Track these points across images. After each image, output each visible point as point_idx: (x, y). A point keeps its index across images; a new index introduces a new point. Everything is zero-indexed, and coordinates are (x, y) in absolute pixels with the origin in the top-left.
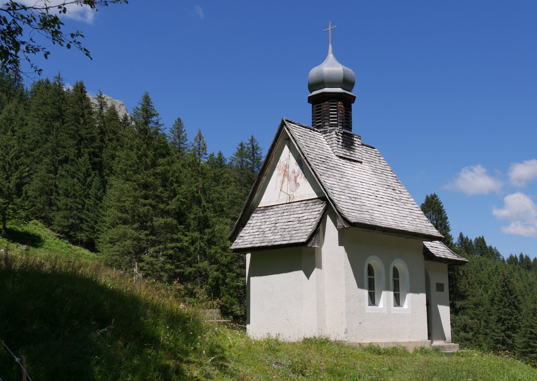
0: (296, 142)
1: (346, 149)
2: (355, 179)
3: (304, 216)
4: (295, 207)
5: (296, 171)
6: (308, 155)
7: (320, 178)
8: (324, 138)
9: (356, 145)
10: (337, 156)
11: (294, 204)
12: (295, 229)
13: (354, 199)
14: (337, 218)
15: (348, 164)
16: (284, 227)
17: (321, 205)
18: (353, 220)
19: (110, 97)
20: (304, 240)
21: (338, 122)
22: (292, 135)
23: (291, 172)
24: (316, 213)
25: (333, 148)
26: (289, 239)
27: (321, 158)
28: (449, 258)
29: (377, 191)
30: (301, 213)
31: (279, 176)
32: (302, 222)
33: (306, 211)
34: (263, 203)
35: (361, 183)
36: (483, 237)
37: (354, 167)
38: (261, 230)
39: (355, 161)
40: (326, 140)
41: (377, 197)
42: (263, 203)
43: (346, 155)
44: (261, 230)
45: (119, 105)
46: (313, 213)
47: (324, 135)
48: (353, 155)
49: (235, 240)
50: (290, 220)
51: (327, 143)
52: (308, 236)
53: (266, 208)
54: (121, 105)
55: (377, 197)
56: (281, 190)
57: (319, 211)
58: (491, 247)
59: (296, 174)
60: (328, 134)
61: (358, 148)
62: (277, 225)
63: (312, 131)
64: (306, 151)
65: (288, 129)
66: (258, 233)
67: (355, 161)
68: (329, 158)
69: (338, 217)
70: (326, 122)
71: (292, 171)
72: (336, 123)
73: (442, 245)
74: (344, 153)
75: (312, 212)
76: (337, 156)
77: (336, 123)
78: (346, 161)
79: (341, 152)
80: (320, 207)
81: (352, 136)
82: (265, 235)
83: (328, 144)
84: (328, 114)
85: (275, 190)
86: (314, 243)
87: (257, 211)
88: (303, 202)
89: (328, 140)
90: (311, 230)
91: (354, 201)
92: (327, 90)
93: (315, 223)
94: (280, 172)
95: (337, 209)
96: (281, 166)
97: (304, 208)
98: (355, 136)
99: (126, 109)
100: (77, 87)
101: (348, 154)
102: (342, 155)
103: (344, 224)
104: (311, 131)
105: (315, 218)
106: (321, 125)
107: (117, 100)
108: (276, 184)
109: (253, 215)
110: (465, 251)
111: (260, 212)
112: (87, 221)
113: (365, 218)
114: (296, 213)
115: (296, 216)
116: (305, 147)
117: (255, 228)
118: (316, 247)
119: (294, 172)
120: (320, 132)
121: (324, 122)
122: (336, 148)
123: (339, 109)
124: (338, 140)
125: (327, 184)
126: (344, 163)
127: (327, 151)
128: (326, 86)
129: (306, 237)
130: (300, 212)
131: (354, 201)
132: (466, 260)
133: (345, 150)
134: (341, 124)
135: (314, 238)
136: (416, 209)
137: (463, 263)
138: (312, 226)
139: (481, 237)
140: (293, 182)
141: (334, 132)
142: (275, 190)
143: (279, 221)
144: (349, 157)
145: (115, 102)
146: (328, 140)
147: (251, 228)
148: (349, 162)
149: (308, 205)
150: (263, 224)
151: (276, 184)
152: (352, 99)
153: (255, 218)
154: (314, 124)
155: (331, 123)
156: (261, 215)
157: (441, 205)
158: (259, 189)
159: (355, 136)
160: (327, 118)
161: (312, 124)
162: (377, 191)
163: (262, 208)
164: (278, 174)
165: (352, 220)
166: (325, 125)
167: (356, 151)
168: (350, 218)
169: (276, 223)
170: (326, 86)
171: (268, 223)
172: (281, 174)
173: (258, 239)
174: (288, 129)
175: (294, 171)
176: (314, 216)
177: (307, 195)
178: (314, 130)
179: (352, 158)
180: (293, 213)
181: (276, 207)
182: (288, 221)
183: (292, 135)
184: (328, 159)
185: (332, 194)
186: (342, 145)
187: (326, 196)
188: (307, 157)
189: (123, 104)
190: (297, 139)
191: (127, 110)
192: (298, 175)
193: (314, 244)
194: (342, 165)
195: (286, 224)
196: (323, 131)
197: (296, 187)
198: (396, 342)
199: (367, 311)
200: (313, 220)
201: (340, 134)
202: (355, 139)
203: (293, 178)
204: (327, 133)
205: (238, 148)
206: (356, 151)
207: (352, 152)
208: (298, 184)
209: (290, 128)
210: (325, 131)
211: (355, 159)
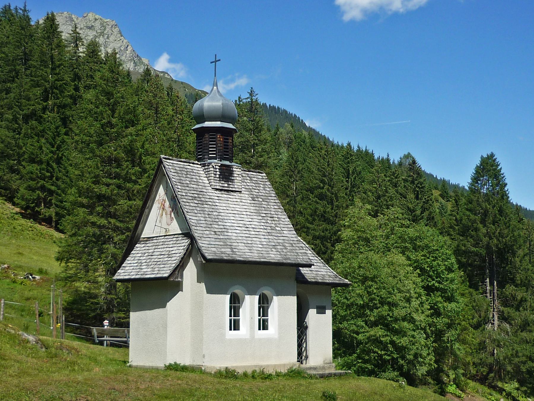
0: (169, 180)
2: (227, 211)
9: (235, 175)
10: (212, 188)
13: (219, 233)
15: (225, 196)
17: (187, 240)
18: (209, 257)
19: (99, 15)
20: (166, 275)
33: (175, 245)
39: (232, 191)
42: (145, 234)
43: (223, 187)
45: (110, 26)
47: (203, 168)
49: (119, 270)
51: (205, 176)
53: (149, 238)
54: (114, 26)
60: (206, 167)
61: (238, 178)
63: (191, 165)
65: (164, 167)
67: (232, 191)
72: (215, 156)
74: (221, 185)
76: (212, 188)
77: (215, 156)
78: (223, 192)
79: (218, 184)
80: (186, 242)
84: (207, 148)
86: (178, 277)
87: (141, 241)
89: (206, 173)
90: (174, 265)
91: (219, 235)
92: (207, 124)
95: (197, 246)
98: (235, 167)
99: (120, 31)
100: (48, 18)
101: (226, 185)
102: (218, 187)
103: (202, 260)
107: (108, 20)
109: (137, 245)
110: (393, 261)
111: (143, 243)
112: (57, 194)
113: (226, 253)
120: (200, 165)
121: (204, 155)
123: (219, 142)
124: (215, 173)
125: (192, 221)
128: (206, 120)
129: (169, 272)
131: (219, 235)
132: (349, 282)
133: (223, 182)
135: (177, 272)
136: (293, 236)
138: (175, 262)
143: (154, 254)
144: (226, 188)
145: (106, 22)
146: (206, 173)
148: (227, 193)
153: (138, 249)
155: (210, 156)
156: (143, 245)
158: (143, 221)
159: (235, 167)
163: (145, 239)
166: (204, 158)
167: (236, 181)
170: (206, 120)
171: (146, 254)
174: (164, 167)
179: (230, 189)
181: (155, 238)
186: (219, 178)
189: (116, 25)
191: (120, 33)
193: (177, 278)
196: (203, 164)
198: (258, 365)
199: (227, 337)
200: (178, 255)
201: (217, 167)
202: (234, 169)
204: (206, 166)
206: (236, 181)
207: (230, 183)
210: (204, 164)
211: (234, 189)
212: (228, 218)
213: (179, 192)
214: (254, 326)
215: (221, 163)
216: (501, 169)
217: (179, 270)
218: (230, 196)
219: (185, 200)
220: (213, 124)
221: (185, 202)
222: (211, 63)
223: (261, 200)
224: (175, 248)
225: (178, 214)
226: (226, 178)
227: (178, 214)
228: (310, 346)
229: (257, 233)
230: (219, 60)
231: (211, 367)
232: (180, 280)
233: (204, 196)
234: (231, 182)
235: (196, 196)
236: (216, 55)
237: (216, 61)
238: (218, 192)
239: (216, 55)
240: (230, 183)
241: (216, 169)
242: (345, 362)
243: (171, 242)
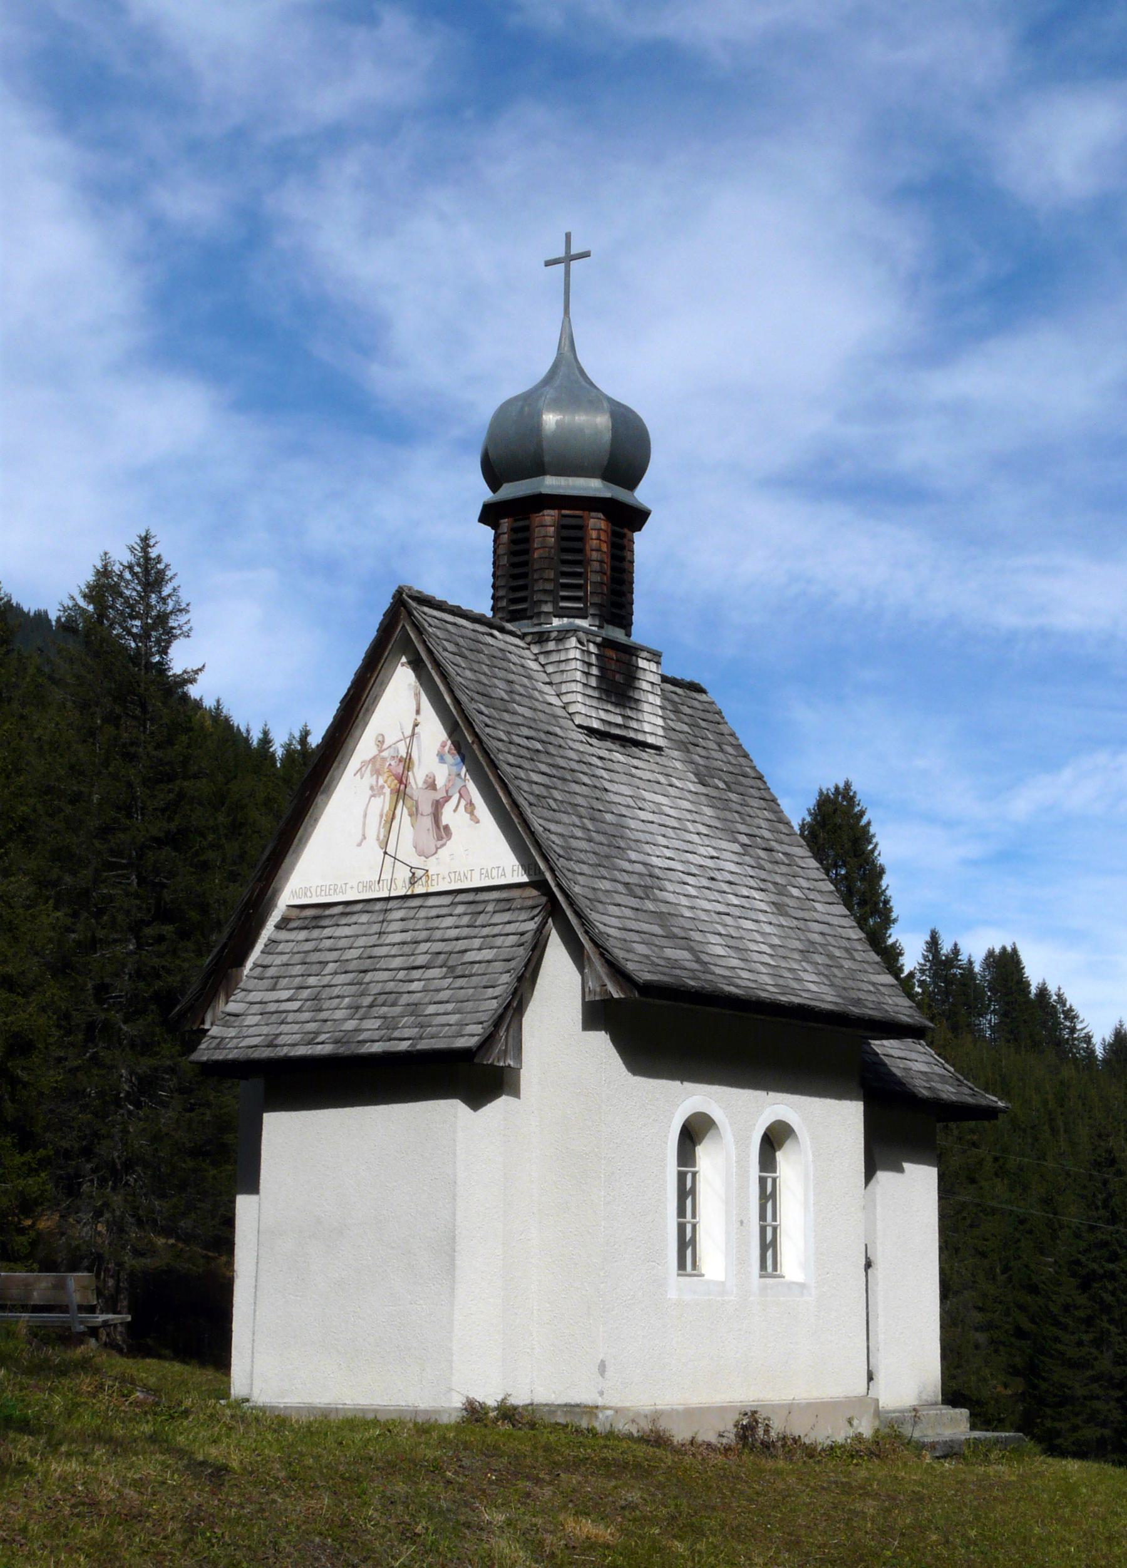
1: (612, 703)
3: (466, 951)
4: (434, 912)
5: (440, 783)
6: (487, 730)
7: (531, 816)
8: (536, 660)
11: (432, 901)
12: (437, 999)
14: (586, 963)
16: (391, 986)
18: (645, 976)
21: (585, 605)
22: (430, 652)
23: (420, 783)
24: (512, 939)
25: (566, 699)
26: (414, 1032)
27: (527, 738)
28: (944, 1096)
29: (712, 858)
30: (457, 939)
31: (373, 796)
32: (459, 971)
34: (313, 890)
35: (663, 830)
36: (1015, 950)
37: (637, 768)
38: (305, 994)
40: (543, 666)
41: (713, 879)
44: (305, 994)
46: (499, 941)
47: (535, 649)
48: (634, 725)
50: (417, 963)
52: (485, 1024)
55: (713, 879)
56: (385, 853)
57: (522, 934)
58: (1043, 992)
59: (439, 795)
62: (368, 977)
63: (496, 633)
64: (481, 713)
66: (296, 1005)
68: (556, 735)
69: (589, 958)
70: (546, 602)
71: (425, 782)
73: (923, 1050)
74: (603, 715)
75: (494, 936)
76: (579, 726)
78: (609, 744)
81: (631, 651)
82: (324, 1015)
83: (550, 683)
85: (359, 845)
88: (460, 898)
90: (494, 1004)
92: (552, 484)
93: (506, 978)
94: (381, 781)
96: (384, 759)
97: (465, 920)
101: (619, 720)
102: (595, 724)
104: (492, 635)
105: (509, 960)
106: (525, 610)
108: (364, 824)
114: (438, 934)
115: (439, 947)
116: (476, 696)
117: (283, 982)
118: (509, 1066)
119: (432, 785)
120: (522, 637)
122: (580, 698)
126: (604, 753)
127: (547, 709)
130: (453, 933)
132: (1001, 1104)
133: (610, 707)
134: (597, 612)
135: (502, 1033)
137: (991, 1113)
138: (497, 991)
139: (1009, 949)
140: (427, 822)
141: (573, 640)
142: (359, 845)
144: (618, 731)
146: (550, 669)
147: (266, 983)
149: (480, 908)
150: (315, 968)
151: (364, 824)
152: (637, 517)
154: (504, 603)
157: (864, 821)
160: (549, 586)
161: (491, 602)
162: (712, 858)
164: (372, 788)
165: (640, 974)
168: (630, 966)
169: (362, 968)
172: (382, 787)
173: (296, 1027)
175: (430, 780)
176: (505, 953)
177: (476, 875)
178: (502, 630)
179: (632, 735)
180: (424, 935)
181: (359, 907)
182: (406, 965)
183: (430, 652)
184: (552, 739)
185: (569, 875)
187: (546, 881)
188: (484, 738)
190: (450, 669)
192: (447, 799)
194: (599, 763)
195: (401, 975)
197: (438, 839)
203: (426, 808)
205: (305, 734)
207: (629, 713)
208: (447, 828)
209: (426, 625)
212: (648, 838)
213: (487, 725)
214: (685, 1261)
215: (603, 633)
216: (869, 823)
217: (510, 1022)
218: (636, 762)
219: (511, 759)
220: (574, 487)
221: (519, 767)
222: (548, 264)
223: (721, 785)
224: (477, 943)
225: (472, 813)
226: (616, 694)
227: (472, 813)
228: (881, 1337)
229: (744, 902)
230: (586, 255)
231: (690, 1413)
232: (512, 1064)
233: (562, 752)
234: (631, 709)
235: (539, 746)
236: (568, 236)
237: (569, 258)
238: (594, 741)
239: (568, 236)
240: (629, 713)
241: (589, 653)
242: (115, 1453)
243: (449, 922)
